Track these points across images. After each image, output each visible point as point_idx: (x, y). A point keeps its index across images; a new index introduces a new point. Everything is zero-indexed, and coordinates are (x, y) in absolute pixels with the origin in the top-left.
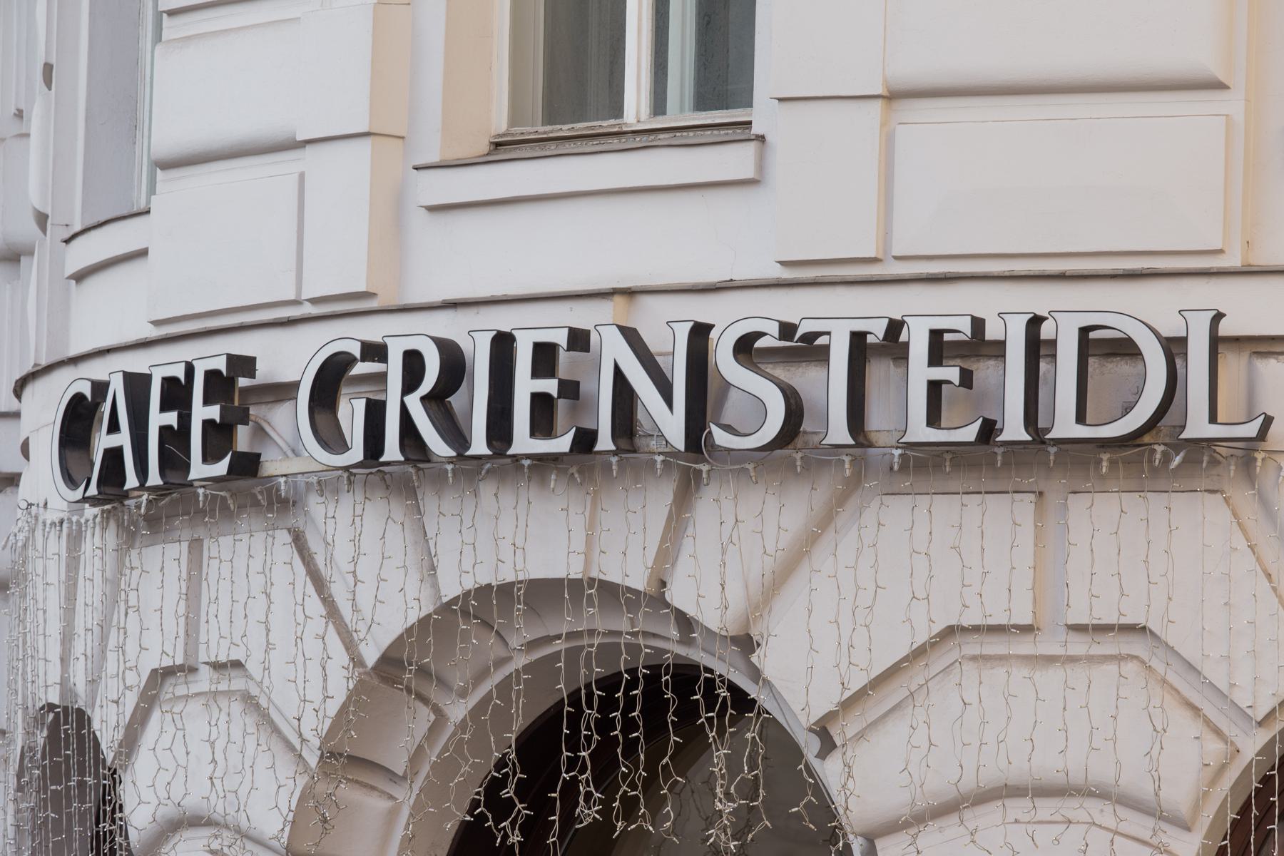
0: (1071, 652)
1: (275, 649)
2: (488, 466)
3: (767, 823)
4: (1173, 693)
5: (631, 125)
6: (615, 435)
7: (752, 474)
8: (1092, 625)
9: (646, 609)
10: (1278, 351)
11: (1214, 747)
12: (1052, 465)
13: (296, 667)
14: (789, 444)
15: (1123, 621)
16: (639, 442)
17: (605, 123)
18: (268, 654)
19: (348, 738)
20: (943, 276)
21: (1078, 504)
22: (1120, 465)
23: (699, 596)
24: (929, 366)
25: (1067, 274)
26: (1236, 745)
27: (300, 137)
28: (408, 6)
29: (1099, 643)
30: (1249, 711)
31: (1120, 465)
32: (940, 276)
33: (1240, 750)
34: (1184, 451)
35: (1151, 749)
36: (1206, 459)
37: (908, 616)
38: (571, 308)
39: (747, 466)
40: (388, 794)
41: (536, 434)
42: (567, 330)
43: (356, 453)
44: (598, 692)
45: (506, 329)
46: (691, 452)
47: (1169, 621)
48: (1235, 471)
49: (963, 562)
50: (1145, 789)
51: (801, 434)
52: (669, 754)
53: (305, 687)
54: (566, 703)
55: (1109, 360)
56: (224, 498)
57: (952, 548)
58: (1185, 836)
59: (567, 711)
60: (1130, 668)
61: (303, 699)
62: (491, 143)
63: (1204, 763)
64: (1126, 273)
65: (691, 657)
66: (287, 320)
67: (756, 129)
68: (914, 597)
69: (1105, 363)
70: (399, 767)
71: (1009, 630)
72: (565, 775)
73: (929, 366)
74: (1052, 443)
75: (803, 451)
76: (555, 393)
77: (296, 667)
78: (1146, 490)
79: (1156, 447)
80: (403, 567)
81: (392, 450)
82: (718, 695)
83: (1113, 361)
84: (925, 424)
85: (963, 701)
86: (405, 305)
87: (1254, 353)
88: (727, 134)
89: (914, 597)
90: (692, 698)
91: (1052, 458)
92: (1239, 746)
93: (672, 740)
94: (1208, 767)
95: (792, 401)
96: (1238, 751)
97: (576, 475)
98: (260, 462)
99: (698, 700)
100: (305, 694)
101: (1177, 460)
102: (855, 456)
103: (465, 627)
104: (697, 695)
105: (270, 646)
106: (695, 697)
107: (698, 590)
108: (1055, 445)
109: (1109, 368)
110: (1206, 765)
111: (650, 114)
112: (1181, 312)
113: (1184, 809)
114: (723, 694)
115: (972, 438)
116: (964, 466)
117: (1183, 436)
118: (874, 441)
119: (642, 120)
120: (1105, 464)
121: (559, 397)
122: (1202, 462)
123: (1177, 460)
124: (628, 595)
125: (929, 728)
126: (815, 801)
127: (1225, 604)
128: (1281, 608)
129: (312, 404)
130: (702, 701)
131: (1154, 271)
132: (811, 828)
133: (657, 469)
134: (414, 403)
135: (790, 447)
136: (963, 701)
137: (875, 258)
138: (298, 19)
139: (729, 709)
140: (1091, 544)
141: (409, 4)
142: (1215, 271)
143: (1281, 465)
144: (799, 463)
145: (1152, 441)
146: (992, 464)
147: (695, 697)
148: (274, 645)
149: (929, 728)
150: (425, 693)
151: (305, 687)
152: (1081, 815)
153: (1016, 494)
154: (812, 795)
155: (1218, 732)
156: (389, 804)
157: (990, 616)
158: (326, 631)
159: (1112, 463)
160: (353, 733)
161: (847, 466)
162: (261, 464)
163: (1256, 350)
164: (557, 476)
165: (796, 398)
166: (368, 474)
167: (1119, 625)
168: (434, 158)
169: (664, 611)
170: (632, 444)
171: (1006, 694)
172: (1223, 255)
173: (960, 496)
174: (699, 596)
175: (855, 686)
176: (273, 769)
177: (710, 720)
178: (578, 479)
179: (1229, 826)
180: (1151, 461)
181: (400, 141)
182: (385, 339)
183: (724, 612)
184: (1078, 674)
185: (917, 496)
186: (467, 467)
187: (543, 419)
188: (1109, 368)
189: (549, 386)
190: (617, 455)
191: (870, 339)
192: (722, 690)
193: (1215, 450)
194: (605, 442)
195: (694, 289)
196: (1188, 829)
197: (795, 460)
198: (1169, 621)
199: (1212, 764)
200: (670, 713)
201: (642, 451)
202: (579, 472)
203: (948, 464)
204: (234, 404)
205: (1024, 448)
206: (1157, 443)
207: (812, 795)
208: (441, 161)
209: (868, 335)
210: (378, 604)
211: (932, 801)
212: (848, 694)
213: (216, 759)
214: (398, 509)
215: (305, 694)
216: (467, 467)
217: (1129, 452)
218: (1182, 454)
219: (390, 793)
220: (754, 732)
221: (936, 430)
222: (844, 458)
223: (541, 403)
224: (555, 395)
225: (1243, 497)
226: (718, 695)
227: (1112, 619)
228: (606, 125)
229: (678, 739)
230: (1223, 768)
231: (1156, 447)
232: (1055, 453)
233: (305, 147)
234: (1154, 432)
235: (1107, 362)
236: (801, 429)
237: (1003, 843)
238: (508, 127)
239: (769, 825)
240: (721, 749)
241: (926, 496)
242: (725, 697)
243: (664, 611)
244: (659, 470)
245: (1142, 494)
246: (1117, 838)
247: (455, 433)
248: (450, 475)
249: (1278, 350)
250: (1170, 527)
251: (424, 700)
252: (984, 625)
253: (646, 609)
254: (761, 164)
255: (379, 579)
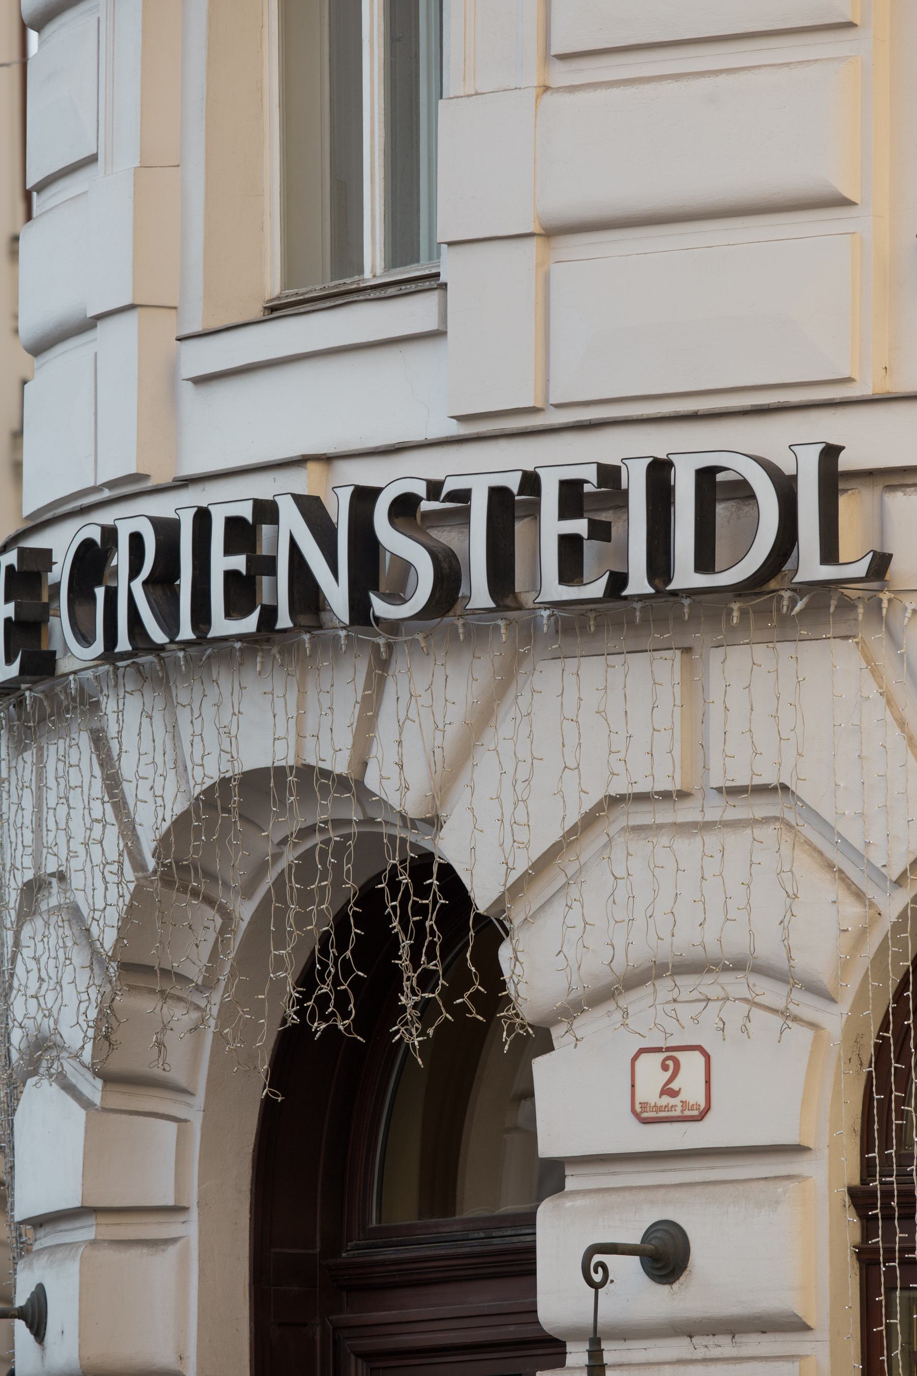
0: (708, 819)
1: (78, 856)
2: (209, 651)
3: (448, 1015)
4: (815, 855)
5: (368, 280)
6: (293, 611)
7: (423, 645)
8: (726, 788)
9: (335, 795)
10: (909, 483)
11: (852, 910)
12: (686, 618)
13: (85, 874)
14: (449, 611)
15: (757, 781)
16: (325, 616)
17: (348, 281)
18: (69, 862)
19: (121, 947)
20: (588, 423)
21: (716, 655)
22: (751, 615)
23: (382, 777)
24: (559, 520)
25: (699, 414)
26: (878, 908)
27: (91, 313)
28: (177, 168)
29: (734, 806)
30: (884, 870)
31: (751, 615)
32: (585, 423)
33: (882, 913)
34: (808, 596)
35: (785, 917)
36: (833, 603)
37: (559, 789)
38: (275, 479)
39: (417, 637)
40: (195, 1004)
41: (232, 614)
42: (595, 466)
43: (98, 647)
44: (297, 886)
45: (662, 456)
46: (359, 624)
47: (798, 779)
48: (864, 614)
49: (610, 728)
50: (779, 959)
51: (460, 600)
52: (350, 948)
53: (93, 895)
54: (412, 893)
55: (747, 503)
56: (41, 700)
57: (597, 712)
58: (834, 1009)
59: (275, 907)
60: (767, 833)
61: (92, 908)
62: (265, 308)
63: (842, 928)
64: (754, 408)
65: (419, 844)
66: (79, 509)
67: (442, 279)
68: (566, 767)
69: (742, 507)
70: (196, 973)
71: (653, 797)
72: (272, 975)
73: (559, 520)
74: (636, 599)
75: (466, 617)
76: (585, 535)
77: (85, 874)
78: (776, 640)
79: (783, 593)
80: (153, 763)
81: (124, 644)
82: (400, 882)
83: (749, 504)
84: (557, 582)
85: (613, 875)
86: (156, 485)
87: (887, 486)
88: (406, 289)
89: (566, 767)
90: (425, 883)
91: (686, 610)
92: (882, 908)
93: (353, 933)
94: (846, 933)
95: (445, 565)
96: (879, 914)
97: (278, 656)
98: (56, 660)
99: (383, 888)
100: (94, 902)
101: (800, 606)
102: (510, 620)
103: (197, 824)
104: (383, 883)
105: (71, 854)
106: (379, 886)
107: (380, 771)
108: (641, 601)
109: (745, 511)
110: (844, 931)
111: (385, 268)
112: (792, 447)
113: (825, 977)
114: (405, 881)
115: (600, 594)
116: (608, 625)
117: (797, 579)
118: (524, 603)
119: (378, 274)
120: (736, 614)
121: (588, 539)
122: (829, 607)
123: (800, 606)
124: (323, 781)
125: (583, 907)
126: (483, 990)
127: (859, 756)
128: (911, 757)
129: (71, 595)
130: (387, 889)
131: (786, 405)
132: (479, 1020)
133: (341, 645)
134: (137, 585)
135: (451, 613)
136: (613, 875)
137: (534, 407)
138: (86, 192)
139: (412, 896)
140: (724, 701)
141: (178, 166)
142: (838, 401)
143: (906, 605)
144: (461, 631)
145: (778, 587)
146: (679, 619)
147: (379, 886)
148: (76, 852)
149: (583, 907)
150: (213, 895)
151: (93, 895)
152: (713, 992)
153: (655, 652)
154: (479, 985)
155: (859, 895)
156: (195, 1015)
157: (635, 783)
158: (103, 834)
159: (743, 613)
160: (125, 942)
161: (503, 631)
162: (58, 661)
163: (889, 484)
164: (262, 657)
165: (450, 561)
166: (126, 667)
167: (752, 786)
168: (197, 328)
169: (345, 795)
170: (318, 619)
171: (652, 866)
172: (854, 383)
173: (604, 657)
174: (382, 777)
175: (522, 866)
176: (74, 984)
177: (394, 908)
178: (183, 668)
179: (891, 997)
180: (779, 610)
181: (173, 311)
182: (669, 456)
183: (403, 793)
184: (737, 842)
185: (567, 660)
186: (565, 615)
187: (233, 610)
188: (745, 511)
189: (579, 526)
190: (689, 597)
191: (587, 488)
192: (404, 877)
193: (842, 593)
194: (284, 621)
195: (376, 451)
196: (833, 1000)
197: (457, 628)
198: (798, 779)
199: (850, 929)
200: (351, 904)
201: (326, 627)
202: (280, 653)
203: (592, 622)
204: (40, 600)
205: (665, 601)
206: (783, 589)
207: (479, 985)
208: (203, 330)
209: (585, 485)
210: (138, 803)
211: (586, 984)
212: (514, 876)
213: (42, 977)
214: (154, 700)
215: (94, 902)
216: (565, 615)
217: (758, 601)
218: (805, 600)
219: (198, 1003)
220: (431, 920)
221: (567, 587)
222: (500, 622)
223: (231, 576)
224: (585, 535)
225: (876, 639)
226: (400, 882)
227: (743, 780)
228: (349, 282)
229: (359, 931)
230: (863, 933)
231: (783, 593)
232: (689, 605)
233: (96, 326)
234: (779, 577)
235: (745, 505)
236: (460, 595)
237: (653, 1025)
238: (281, 290)
239: (450, 1018)
240: (405, 940)
241: (573, 659)
242: (407, 884)
243: (345, 795)
244: (343, 646)
245: (770, 645)
246: (756, 1013)
247: (170, 623)
248: (182, 663)
249: (910, 482)
250: (797, 678)
251: (210, 901)
252: (630, 794)
253: (335, 795)
254: (443, 316)
255: (138, 778)
